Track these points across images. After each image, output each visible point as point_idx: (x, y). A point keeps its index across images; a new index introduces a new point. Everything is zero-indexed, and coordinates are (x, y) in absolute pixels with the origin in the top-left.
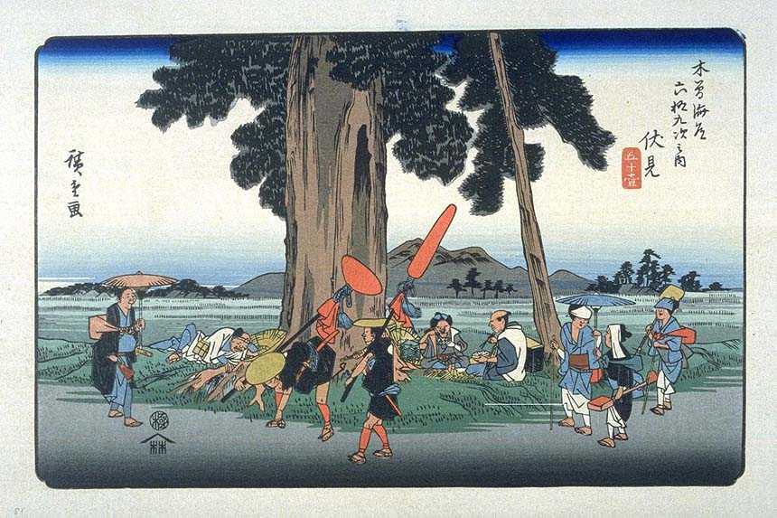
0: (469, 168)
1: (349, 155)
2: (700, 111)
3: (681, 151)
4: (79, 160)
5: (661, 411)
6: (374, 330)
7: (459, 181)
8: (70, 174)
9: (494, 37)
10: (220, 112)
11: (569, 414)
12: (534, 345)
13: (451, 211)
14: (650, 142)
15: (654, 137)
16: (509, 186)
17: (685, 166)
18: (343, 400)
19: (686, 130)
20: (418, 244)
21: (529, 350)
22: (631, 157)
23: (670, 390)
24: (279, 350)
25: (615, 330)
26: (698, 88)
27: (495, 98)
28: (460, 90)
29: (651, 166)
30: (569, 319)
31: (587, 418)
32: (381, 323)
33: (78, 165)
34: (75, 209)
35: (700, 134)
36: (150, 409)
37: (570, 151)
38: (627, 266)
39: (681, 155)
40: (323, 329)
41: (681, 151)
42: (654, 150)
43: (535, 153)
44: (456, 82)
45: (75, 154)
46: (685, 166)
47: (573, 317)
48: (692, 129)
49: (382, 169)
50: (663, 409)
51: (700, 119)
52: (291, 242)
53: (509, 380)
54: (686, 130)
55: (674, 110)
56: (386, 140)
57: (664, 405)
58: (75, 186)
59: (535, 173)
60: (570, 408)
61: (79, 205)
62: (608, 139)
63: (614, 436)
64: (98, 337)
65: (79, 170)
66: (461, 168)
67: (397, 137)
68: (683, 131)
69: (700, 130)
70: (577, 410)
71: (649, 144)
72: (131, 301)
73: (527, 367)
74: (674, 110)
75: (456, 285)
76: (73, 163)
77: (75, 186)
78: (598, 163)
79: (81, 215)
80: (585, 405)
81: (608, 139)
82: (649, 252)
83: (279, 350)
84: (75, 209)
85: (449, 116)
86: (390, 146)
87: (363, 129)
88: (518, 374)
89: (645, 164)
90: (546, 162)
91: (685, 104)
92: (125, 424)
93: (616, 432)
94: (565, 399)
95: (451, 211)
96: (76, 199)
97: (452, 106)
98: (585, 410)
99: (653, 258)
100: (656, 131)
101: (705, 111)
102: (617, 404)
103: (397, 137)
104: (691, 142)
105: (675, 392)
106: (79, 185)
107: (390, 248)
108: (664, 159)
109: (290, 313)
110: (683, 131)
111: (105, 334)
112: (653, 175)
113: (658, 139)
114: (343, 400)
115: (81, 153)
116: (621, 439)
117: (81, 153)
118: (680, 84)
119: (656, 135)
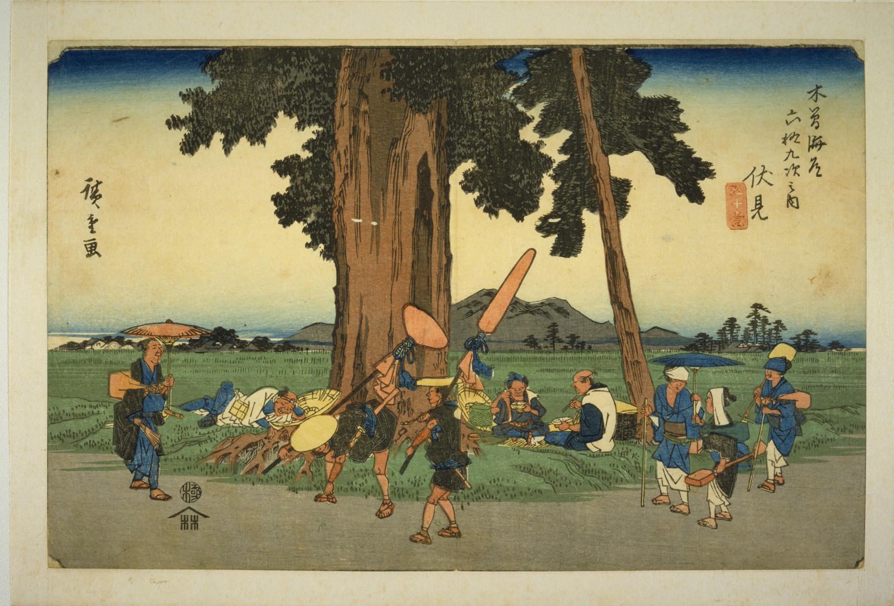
0: (546, 204)
1: (410, 186)
2: (817, 143)
3: (793, 190)
4: (97, 191)
5: (772, 487)
6: (439, 389)
7: (532, 219)
8: (87, 206)
9: (576, 54)
10: (258, 136)
11: (664, 490)
12: (625, 408)
13: (532, 253)
14: (757, 179)
15: (762, 174)
16: (591, 220)
17: (798, 207)
18: (402, 470)
19: (799, 166)
20: (491, 294)
21: (620, 417)
22: (734, 190)
23: (782, 462)
24: (331, 412)
25: (717, 394)
26: (813, 117)
27: (575, 123)
28: (536, 113)
29: (759, 206)
30: (664, 381)
31: (684, 496)
32: (448, 381)
33: (96, 197)
34: (92, 249)
35: (815, 170)
36: (180, 480)
37: (666, 185)
38: (732, 322)
39: (792, 195)
40: (381, 388)
41: (793, 190)
42: (761, 189)
43: (622, 187)
44: (530, 104)
45: (93, 184)
46: (798, 207)
47: (669, 379)
48: (805, 165)
49: (445, 207)
50: (774, 484)
51: (814, 152)
52: (341, 293)
53: (594, 450)
54: (799, 166)
55: (784, 142)
56: (452, 168)
57: (774, 480)
58: (93, 221)
59: (622, 208)
60: (665, 483)
61: (96, 243)
62: (705, 170)
63: (716, 514)
64: (122, 395)
65: (98, 202)
66: (535, 207)
67: (469, 165)
68: (796, 168)
69: (814, 164)
70: (673, 486)
71: (755, 183)
72: (159, 354)
73: (618, 436)
74: (784, 142)
75: (532, 342)
76: (90, 194)
77: (93, 221)
78: (696, 196)
79: (99, 255)
80: (683, 479)
81: (705, 170)
82: (757, 306)
83: (331, 412)
84: (92, 249)
85: (459, 155)
86: (456, 178)
87: (425, 156)
88: (605, 444)
89: (751, 205)
90: (632, 198)
91: (798, 135)
92: (150, 496)
93: (718, 511)
94: (660, 474)
95: (532, 253)
96: (92, 236)
97: (452, 140)
98: (682, 485)
99: (762, 313)
100: (763, 166)
101: (822, 144)
102: (719, 477)
103: (469, 165)
104: (805, 180)
105: (788, 465)
106: (97, 220)
107: (454, 302)
108: (774, 200)
109: (341, 367)
110: (796, 168)
111: (130, 393)
112: (760, 218)
113: (765, 176)
114: (402, 472)
115: (99, 183)
116: (724, 518)
117: (99, 183)
118: (792, 112)
119: (764, 172)
